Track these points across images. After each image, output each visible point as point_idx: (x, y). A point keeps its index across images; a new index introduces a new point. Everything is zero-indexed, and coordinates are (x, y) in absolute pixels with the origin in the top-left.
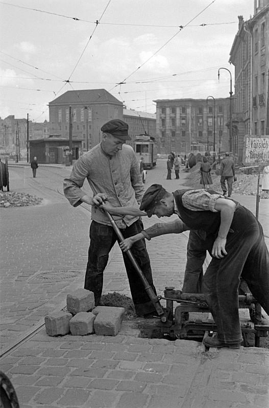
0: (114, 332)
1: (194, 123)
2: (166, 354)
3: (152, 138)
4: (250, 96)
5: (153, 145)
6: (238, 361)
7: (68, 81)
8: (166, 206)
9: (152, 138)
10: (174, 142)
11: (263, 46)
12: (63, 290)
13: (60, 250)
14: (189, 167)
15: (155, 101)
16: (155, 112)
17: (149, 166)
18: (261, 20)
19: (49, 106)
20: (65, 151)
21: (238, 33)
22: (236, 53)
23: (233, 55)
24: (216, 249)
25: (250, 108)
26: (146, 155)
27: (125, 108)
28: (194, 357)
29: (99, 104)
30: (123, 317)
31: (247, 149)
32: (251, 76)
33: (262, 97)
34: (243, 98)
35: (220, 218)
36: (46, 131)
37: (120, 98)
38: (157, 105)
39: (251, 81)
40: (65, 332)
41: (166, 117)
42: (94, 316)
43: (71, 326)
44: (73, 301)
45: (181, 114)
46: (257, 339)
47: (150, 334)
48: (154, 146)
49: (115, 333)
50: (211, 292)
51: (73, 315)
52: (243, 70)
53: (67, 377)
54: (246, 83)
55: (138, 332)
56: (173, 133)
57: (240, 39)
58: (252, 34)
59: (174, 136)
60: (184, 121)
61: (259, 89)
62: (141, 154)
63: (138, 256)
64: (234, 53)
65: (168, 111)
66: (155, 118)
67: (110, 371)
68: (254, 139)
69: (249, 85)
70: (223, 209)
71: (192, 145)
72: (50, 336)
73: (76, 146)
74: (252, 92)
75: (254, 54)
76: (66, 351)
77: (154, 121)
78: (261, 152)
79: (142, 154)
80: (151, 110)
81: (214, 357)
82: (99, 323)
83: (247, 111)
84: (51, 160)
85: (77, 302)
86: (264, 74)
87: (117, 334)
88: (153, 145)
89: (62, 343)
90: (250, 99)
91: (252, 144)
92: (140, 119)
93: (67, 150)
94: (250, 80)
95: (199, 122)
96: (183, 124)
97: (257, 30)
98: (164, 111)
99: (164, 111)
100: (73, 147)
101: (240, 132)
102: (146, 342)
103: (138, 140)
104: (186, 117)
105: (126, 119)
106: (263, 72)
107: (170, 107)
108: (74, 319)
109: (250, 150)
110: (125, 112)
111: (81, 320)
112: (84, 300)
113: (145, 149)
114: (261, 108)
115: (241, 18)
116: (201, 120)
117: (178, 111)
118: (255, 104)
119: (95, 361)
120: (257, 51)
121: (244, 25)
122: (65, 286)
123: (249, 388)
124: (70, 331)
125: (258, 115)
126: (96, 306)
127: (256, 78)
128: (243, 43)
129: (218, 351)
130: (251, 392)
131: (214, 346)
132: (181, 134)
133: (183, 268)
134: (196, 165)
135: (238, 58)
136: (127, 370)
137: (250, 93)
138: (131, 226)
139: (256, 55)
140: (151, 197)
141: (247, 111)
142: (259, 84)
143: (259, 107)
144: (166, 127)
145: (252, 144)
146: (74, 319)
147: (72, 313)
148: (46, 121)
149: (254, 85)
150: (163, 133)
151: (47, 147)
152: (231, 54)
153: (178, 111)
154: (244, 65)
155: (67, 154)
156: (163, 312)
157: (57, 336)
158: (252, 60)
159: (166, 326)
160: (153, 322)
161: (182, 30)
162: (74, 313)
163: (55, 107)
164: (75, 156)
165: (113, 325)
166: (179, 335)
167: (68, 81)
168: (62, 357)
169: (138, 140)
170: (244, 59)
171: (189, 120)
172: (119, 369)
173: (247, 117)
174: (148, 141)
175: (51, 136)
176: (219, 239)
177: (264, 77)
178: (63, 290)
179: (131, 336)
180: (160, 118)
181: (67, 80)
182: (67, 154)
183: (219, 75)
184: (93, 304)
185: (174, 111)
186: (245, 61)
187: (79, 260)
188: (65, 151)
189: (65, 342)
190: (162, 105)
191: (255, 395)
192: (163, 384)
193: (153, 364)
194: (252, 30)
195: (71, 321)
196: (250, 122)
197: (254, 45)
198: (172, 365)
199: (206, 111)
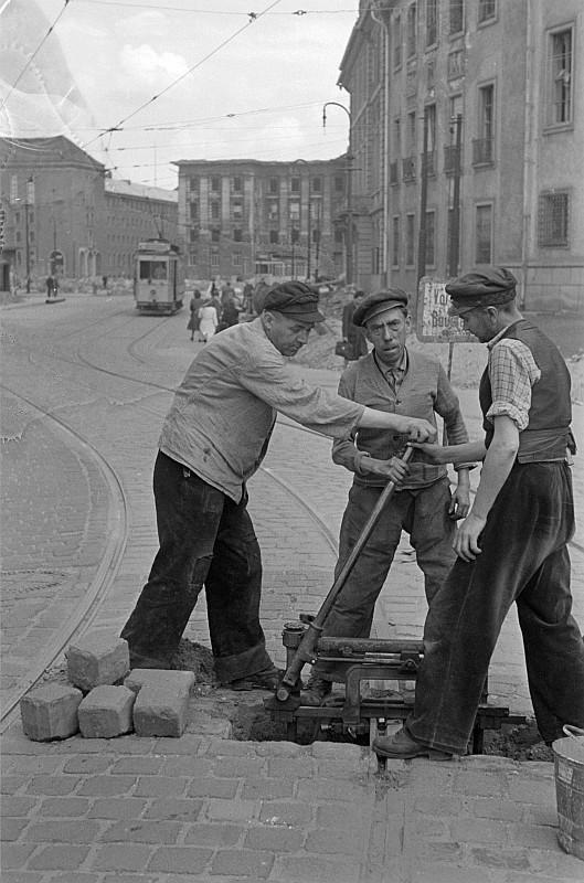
1: (261, 213)
2: (300, 778)
3: (174, 248)
5: (176, 262)
6: (454, 791)
9: (174, 248)
11: (413, 54)
14: (255, 313)
15: (176, 164)
16: (176, 185)
17: (169, 308)
21: (357, 24)
25: (383, 187)
26: (162, 284)
27: (110, 176)
30: (192, 692)
32: (386, 117)
33: (409, 164)
34: (369, 164)
37: (99, 157)
38: (180, 172)
40: (68, 732)
42: (131, 693)
43: (81, 718)
44: (84, 662)
45: (231, 193)
46: (478, 734)
48: (180, 265)
51: (85, 693)
52: (368, 105)
53: (95, 846)
55: (225, 727)
56: (216, 233)
58: (388, 25)
60: (238, 209)
61: (403, 146)
62: (150, 282)
64: (348, 66)
65: (204, 185)
66: (175, 199)
67: (189, 825)
71: (258, 263)
74: (389, 152)
75: (393, 71)
77: (175, 206)
79: (154, 281)
80: (164, 182)
82: (144, 710)
85: (92, 663)
86: (413, 115)
88: (176, 262)
91: (436, 296)
92: (146, 201)
95: (270, 210)
96: (237, 215)
97: (398, 19)
98: (194, 186)
99: (194, 186)
101: (360, 237)
103: (143, 252)
104: (242, 199)
105: (111, 201)
106: (410, 111)
108: (87, 703)
109: (432, 310)
110: (109, 187)
111: (104, 704)
112: (108, 659)
113: (159, 271)
116: (274, 208)
117: (226, 185)
118: (394, 178)
119: (150, 801)
120: (398, 63)
121: (372, 7)
123: (489, 855)
125: (402, 202)
128: (368, 46)
130: (498, 866)
131: (397, 755)
135: (358, 77)
136: (225, 824)
137: (383, 154)
139: (396, 72)
141: (378, 193)
142: (403, 135)
143: (403, 184)
145: (436, 296)
146: (87, 703)
147: (80, 688)
149: (392, 139)
150: (194, 235)
152: (348, 75)
153: (226, 185)
154: (371, 94)
159: (284, 706)
160: (258, 698)
161: (255, 21)
162: (86, 688)
168: (71, 795)
169: (143, 252)
171: (249, 206)
172: (205, 822)
173: (377, 205)
174: (166, 253)
177: (413, 122)
178: (36, 620)
180: (188, 200)
183: (324, 117)
185: (216, 186)
186: (372, 87)
187: (56, 544)
189: (69, 756)
190: (191, 171)
191: (506, 872)
192: (310, 854)
193: (275, 805)
194: (389, 18)
196: (383, 217)
198: (317, 805)
199: (285, 186)
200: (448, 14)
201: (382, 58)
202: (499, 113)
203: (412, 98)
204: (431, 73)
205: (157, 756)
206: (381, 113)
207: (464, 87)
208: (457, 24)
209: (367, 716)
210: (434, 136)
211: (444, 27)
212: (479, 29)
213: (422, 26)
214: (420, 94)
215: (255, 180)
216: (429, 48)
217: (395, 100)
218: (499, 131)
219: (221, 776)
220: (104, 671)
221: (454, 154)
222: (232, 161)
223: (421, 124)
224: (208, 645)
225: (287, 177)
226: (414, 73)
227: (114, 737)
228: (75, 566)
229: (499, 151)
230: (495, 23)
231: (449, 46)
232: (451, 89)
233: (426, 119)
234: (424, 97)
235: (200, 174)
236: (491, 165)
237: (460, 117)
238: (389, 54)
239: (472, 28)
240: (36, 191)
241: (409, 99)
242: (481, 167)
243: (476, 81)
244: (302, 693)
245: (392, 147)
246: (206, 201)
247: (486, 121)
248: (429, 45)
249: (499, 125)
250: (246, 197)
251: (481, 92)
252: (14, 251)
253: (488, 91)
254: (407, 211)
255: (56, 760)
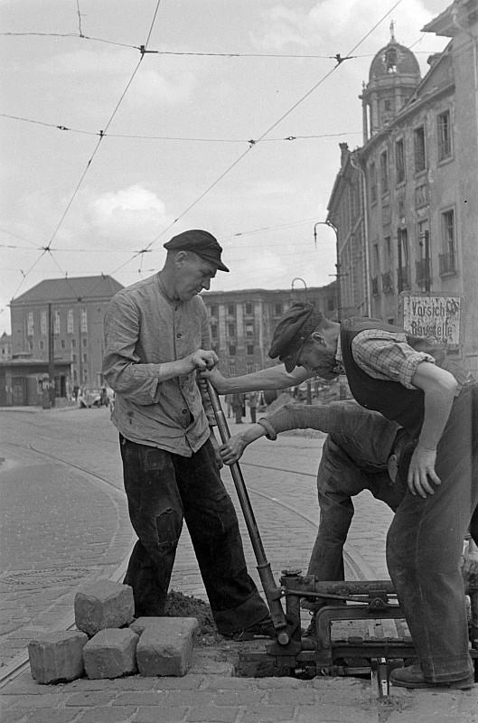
0: (179, 667)
2: (301, 705)
4: (366, 277)
7: (48, 249)
8: (325, 345)
10: (234, 364)
11: (386, 190)
12: (59, 601)
13: (44, 536)
14: (265, 405)
18: (379, 149)
19: (11, 306)
20: (40, 382)
22: (338, 205)
23: (333, 209)
24: (417, 471)
25: (367, 298)
28: (362, 709)
29: (99, 301)
30: (196, 638)
31: (406, 319)
33: (387, 279)
35: (424, 409)
36: (6, 352)
39: (367, 252)
41: (218, 323)
42: (134, 635)
43: (86, 659)
45: (244, 316)
47: (254, 671)
49: (183, 670)
50: (403, 568)
51: (90, 637)
52: (352, 235)
54: (358, 256)
56: (233, 350)
57: (344, 182)
59: (234, 354)
60: (250, 329)
61: (382, 264)
63: (215, 511)
68: (417, 299)
69: (363, 259)
70: (430, 391)
72: (40, 684)
73: (61, 374)
75: (371, 205)
76: (81, 711)
78: (431, 324)
81: (404, 706)
83: (363, 304)
84: (15, 400)
85: (97, 607)
86: (388, 239)
87: (186, 674)
89: (69, 696)
90: (366, 283)
91: (414, 309)
93: (45, 379)
94: (365, 251)
96: (249, 333)
97: (373, 165)
100: (56, 375)
102: (251, 685)
104: (253, 320)
107: (224, 304)
108: (91, 644)
111: (108, 643)
114: (387, 296)
115: (344, 146)
117: (240, 310)
118: (375, 291)
121: (351, 157)
122: (62, 595)
124: (84, 670)
125: (383, 310)
126: (136, 616)
127: (376, 246)
129: (409, 694)
132: (247, 351)
133: (313, 535)
134: (277, 400)
138: (198, 451)
140: (291, 327)
141: (363, 304)
143: (383, 295)
144: (219, 340)
145: (414, 309)
146: (91, 644)
147: (87, 633)
148: (5, 334)
149: (372, 259)
151: (9, 376)
154: (353, 225)
155: (45, 387)
156: (285, 624)
157: (55, 682)
158: (368, 216)
160: (260, 647)
162: (92, 633)
163: (21, 308)
164: (59, 392)
165: (178, 653)
166: (327, 670)
167: (48, 249)
170: (353, 215)
175: (14, 357)
176: (419, 450)
178: (59, 601)
179: (216, 672)
181: (45, 247)
182: (45, 387)
184: (130, 612)
185: (232, 311)
186: (354, 220)
188: (40, 382)
195: (84, 649)
197: (370, 193)
200: (413, 158)
201: (361, 197)
202: (459, 232)
203: (387, 225)
204: (401, 204)
205: (159, 691)
206: (363, 239)
207: (429, 214)
208: (421, 164)
209: (368, 656)
210: (407, 254)
211: (410, 169)
212: (441, 166)
213: (392, 168)
214: (393, 222)
215: (263, 306)
216: (399, 185)
217: (374, 228)
218: (460, 244)
219: (221, 705)
220: (110, 614)
221: (424, 268)
222: (244, 291)
223: (395, 242)
224: (206, 600)
225: (289, 302)
226: (388, 206)
227: (118, 677)
228: (99, 565)
229: (461, 261)
230: (452, 161)
231: (414, 182)
232: (418, 215)
233: (399, 238)
234: (396, 223)
235: (219, 302)
236: (455, 274)
237: (427, 233)
238: (367, 192)
239: (433, 166)
240: (89, 319)
241: (384, 226)
242: (448, 276)
243: (438, 209)
244: (302, 639)
245: (373, 267)
246: (224, 323)
247: (449, 239)
248: (398, 183)
249: (460, 241)
250: (256, 319)
251: (443, 218)
252: (69, 365)
253: (449, 216)
254: (387, 316)
255: (59, 698)
